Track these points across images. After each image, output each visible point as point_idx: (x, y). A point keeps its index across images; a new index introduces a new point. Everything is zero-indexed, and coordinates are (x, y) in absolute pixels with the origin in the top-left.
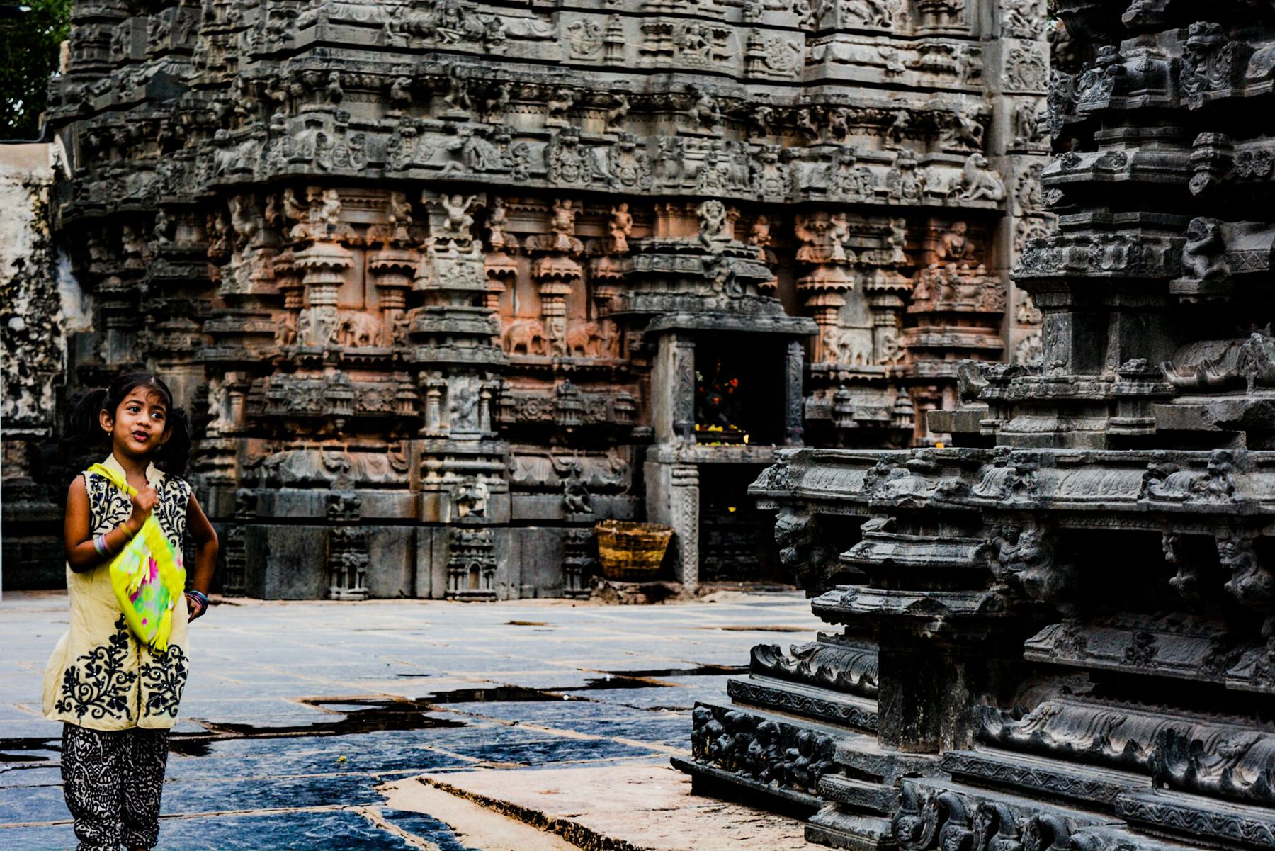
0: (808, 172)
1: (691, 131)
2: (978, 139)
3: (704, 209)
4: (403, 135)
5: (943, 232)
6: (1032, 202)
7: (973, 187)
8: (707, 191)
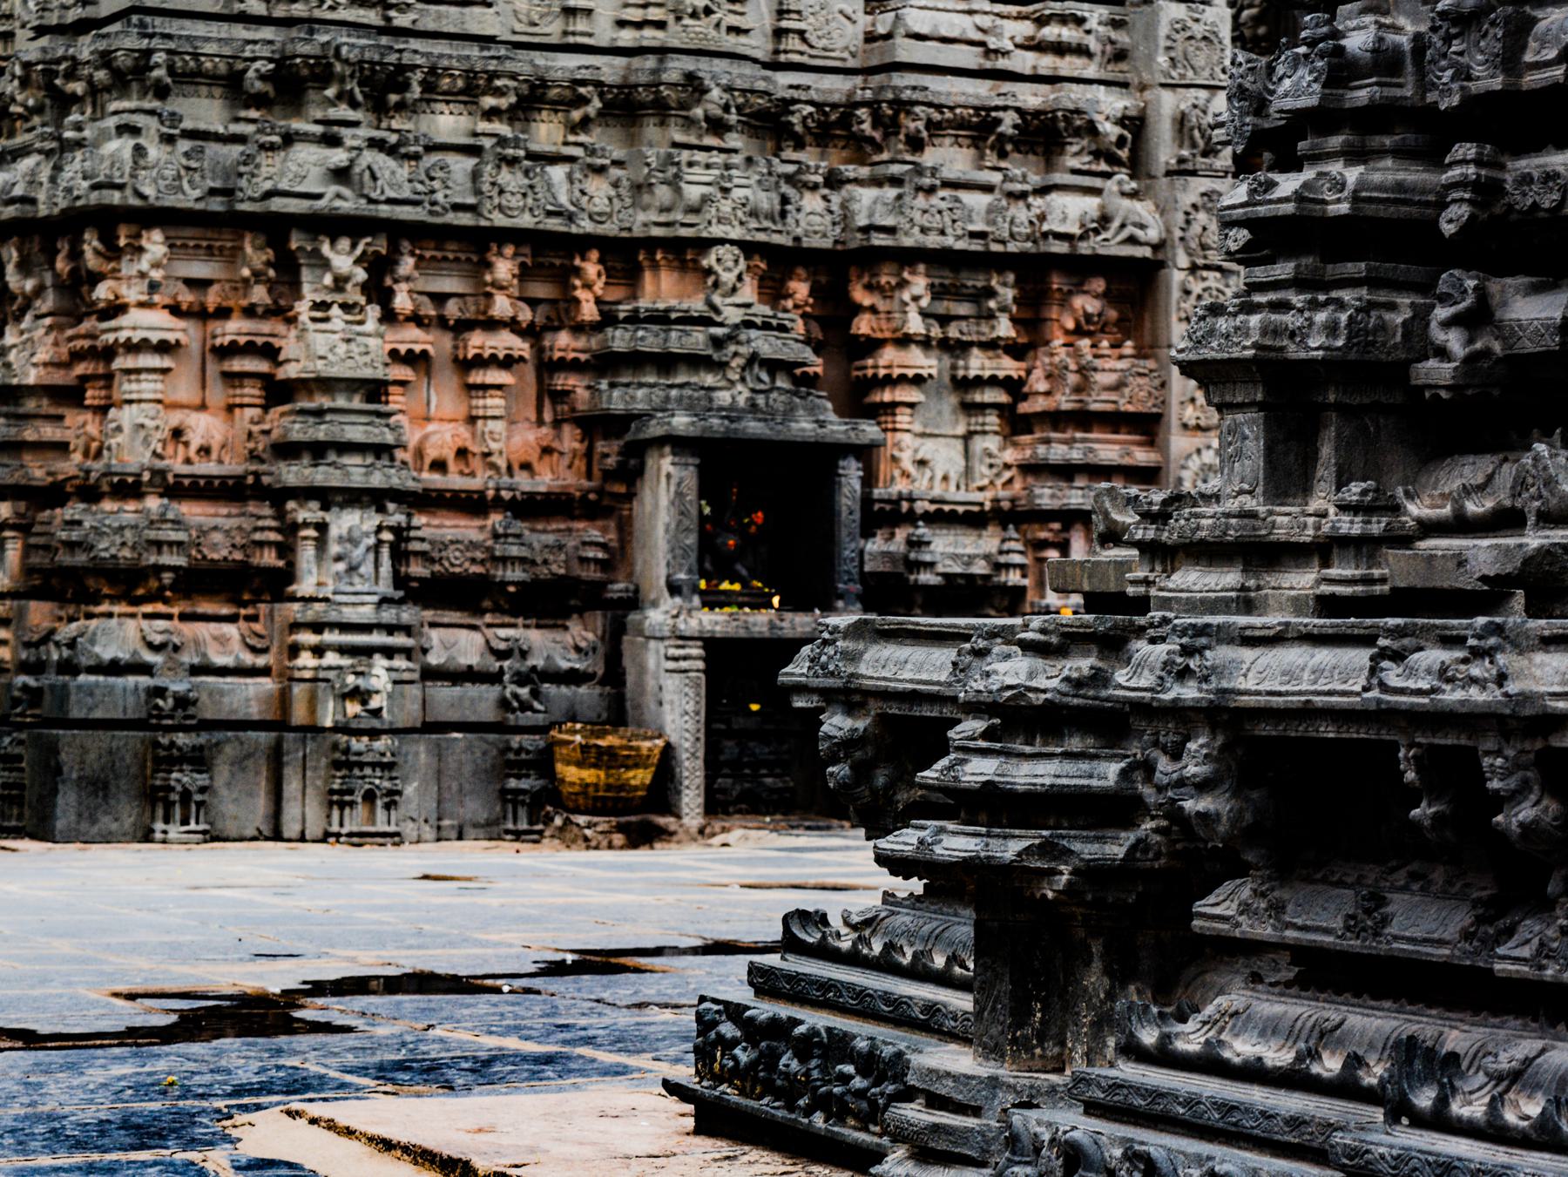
0: (868, 203)
1: (693, 140)
2: (1124, 154)
3: (713, 257)
4: (262, 147)
5: (1070, 293)
6: (1204, 247)
7: (1116, 224)
8: (717, 231)
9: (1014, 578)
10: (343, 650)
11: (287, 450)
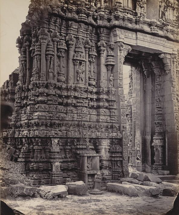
9: (110, 166)
10: (57, 176)
11: (52, 158)
